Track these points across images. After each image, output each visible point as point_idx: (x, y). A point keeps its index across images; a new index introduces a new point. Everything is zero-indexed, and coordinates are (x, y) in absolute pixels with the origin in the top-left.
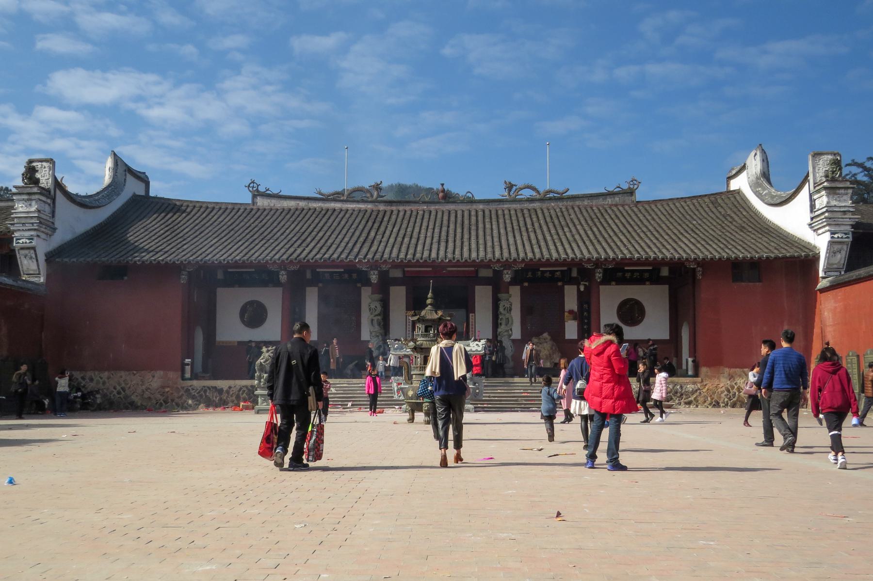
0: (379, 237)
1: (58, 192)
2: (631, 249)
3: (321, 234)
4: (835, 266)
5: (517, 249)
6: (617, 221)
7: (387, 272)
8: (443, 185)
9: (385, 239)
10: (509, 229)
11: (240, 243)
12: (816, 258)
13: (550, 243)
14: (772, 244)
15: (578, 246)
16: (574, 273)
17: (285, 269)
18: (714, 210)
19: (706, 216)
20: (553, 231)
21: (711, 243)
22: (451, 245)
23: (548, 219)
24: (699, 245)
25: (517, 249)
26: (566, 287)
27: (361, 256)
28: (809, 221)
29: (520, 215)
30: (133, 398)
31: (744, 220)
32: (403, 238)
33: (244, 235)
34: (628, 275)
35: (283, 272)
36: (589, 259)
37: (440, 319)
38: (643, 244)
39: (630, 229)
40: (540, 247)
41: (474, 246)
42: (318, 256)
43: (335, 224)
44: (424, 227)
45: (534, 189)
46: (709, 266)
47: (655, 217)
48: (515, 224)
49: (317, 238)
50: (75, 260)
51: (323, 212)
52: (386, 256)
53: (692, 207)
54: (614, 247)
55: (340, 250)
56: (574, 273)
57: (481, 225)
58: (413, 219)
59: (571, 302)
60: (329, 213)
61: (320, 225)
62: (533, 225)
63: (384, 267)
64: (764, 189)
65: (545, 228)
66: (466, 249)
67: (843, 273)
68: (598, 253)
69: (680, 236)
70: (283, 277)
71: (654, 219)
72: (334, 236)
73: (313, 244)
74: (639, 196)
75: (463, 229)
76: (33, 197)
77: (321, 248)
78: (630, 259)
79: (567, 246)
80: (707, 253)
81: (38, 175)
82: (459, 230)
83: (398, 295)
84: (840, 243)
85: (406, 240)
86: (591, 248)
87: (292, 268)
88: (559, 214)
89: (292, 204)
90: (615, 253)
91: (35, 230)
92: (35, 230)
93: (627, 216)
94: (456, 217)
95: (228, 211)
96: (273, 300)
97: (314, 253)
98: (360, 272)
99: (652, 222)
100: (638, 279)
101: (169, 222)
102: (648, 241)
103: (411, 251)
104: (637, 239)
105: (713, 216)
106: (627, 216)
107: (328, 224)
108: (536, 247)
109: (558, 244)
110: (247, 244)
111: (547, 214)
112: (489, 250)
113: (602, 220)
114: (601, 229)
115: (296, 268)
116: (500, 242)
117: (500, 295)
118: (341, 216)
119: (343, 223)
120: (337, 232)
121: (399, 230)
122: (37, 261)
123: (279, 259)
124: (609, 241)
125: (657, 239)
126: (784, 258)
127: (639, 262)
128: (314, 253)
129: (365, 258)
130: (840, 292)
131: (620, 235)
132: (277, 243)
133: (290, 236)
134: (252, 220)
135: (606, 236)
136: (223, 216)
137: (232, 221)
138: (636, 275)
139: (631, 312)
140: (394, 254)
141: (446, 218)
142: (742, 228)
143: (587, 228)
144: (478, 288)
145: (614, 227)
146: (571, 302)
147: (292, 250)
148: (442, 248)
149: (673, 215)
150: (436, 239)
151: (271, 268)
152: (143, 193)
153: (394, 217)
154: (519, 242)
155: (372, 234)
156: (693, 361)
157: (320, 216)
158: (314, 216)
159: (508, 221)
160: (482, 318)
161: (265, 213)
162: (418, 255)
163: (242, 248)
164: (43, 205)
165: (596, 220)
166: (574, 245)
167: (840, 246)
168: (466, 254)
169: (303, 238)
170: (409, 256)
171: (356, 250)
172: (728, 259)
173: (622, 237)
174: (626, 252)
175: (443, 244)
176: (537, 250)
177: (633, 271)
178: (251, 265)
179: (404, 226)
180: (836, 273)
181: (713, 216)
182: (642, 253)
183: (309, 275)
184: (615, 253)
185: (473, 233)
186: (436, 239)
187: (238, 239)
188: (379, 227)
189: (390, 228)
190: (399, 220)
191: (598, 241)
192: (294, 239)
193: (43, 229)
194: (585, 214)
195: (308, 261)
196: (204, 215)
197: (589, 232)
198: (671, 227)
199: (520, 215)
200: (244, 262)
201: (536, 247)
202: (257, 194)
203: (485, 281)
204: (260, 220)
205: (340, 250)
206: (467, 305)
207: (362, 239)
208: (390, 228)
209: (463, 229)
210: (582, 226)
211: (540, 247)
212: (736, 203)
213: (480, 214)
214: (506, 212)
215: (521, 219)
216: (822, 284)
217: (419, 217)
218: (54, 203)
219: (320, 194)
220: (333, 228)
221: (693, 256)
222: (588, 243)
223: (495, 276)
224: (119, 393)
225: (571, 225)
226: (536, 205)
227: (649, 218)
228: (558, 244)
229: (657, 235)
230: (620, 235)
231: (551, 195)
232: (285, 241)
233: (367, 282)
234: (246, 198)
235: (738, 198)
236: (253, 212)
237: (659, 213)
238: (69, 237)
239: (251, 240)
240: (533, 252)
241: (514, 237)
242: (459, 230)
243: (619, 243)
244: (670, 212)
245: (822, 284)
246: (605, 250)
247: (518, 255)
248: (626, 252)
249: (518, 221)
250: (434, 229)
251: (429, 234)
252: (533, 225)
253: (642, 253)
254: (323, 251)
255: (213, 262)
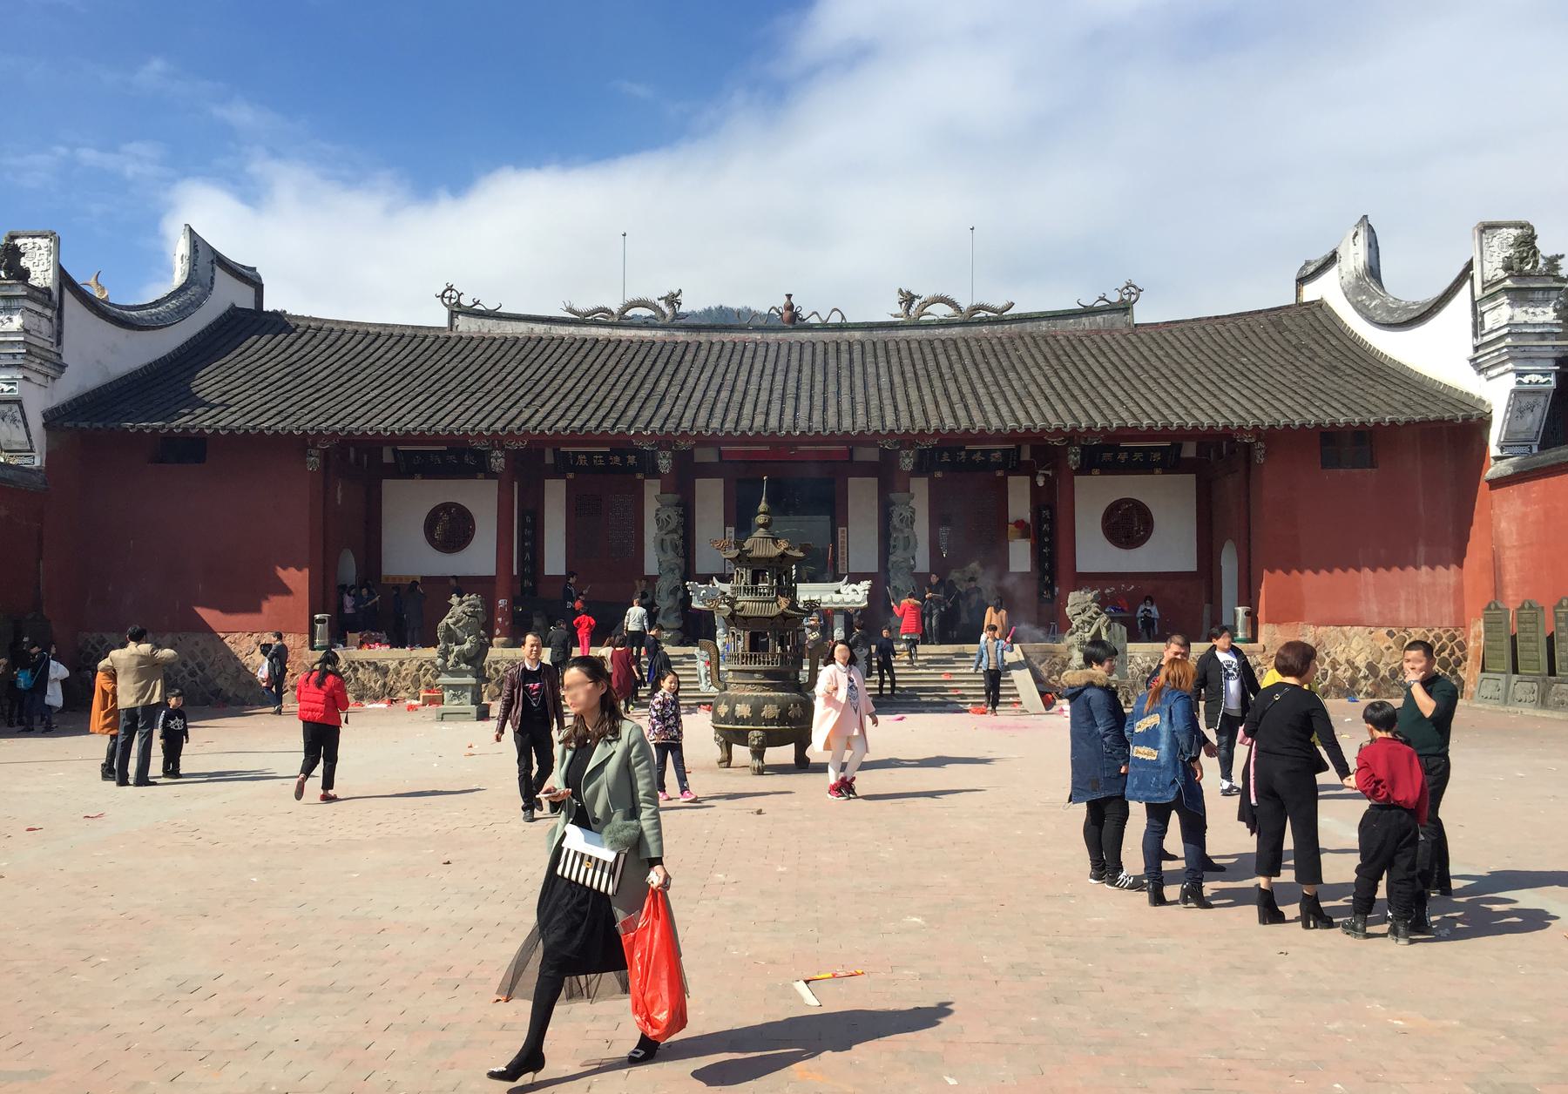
0: (674, 390)
1: (67, 295)
2: (1135, 410)
3: (569, 384)
4: (1522, 436)
5: (925, 412)
6: (1102, 359)
7: (690, 453)
8: (789, 296)
9: (684, 394)
10: (909, 375)
11: (420, 399)
12: (1485, 422)
13: (985, 400)
14: (1397, 397)
15: (1037, 405)
16: (1026, 455)
17: (502, 448)
18: (1277, 337)
19: (1262, 347)
20: (988, 379)
21: (1280, 396)
22: (804, 402)
23: (978, 357)
24: (1258, 401)
25: (925, 412)
26: (1011, 479)
27: (640, 425)
28: (1470, 353)
29: (927, 350)
30: (220, 682)
31: (1336, 354)
32: (718, 392)
33: (428, 383)
34: (1123, 457)
35: (497, 453)
36: (1058, 429)
37: (783, 555)
38: (1154, 400)
39: (1128, 374)
40: (966, 407)
41: (846, 405)
42: (561, 424)
43: (597, 366)
44: (756, 372)
45: (951, 303)
46: (1278, 438)
47: (1172, 352)
48: (919, 366)
49: (563, 391)
50: (100, 425)
51: (577, 345)
52: (686, 424)
53: (1236, 332)
54: (1102, 406)
55: (602, 412)
56: (1026, 455)
57: (858, 369)
58: (736, 358)
59: (1019, 506)
60: (588, 346)
61: (569, 368)
62: (951, 367)
63: (683, 445)
64: (1372, 298)
65: (974, 374)
66: (832, 411)
67: (1535, 450)
68: (1074, 417)
69: (1222, 385)
70: (498, 462)
71: (1167, 355)
72: (592, 388)
73: (553, 402)
74: (1144, 314)
75: (826, 374)
76: (15, 303)
77: (568, 409)
78: (1135, 428)
79: (1016, 405)
80: (1278, 416)
81: (24, 262)
82: (819, 377)
83: (710, 496)
84: (1533, 392)
85: (724, 394)
86: (1060, 408)
87: (514, 446)
88: (998, 348)
89: (521, 329)
90: (1104, 416)
91: (20, 366)
92: (20, 366)
93: (1119, 351)
94: (814, 354)
95: (406, 340)
96: (481, 501)
97: (553, 417)
98: (638, 452)
99: (1166, 360)
100: (1142, 463)
101: (295, 358)
102: (1163, 395)
103: (732, 415)
104: (1143, 390)
105: (1276, 348)
106: (1119, 351)
107: (585, 366)
108: (959, 408)
109: (1000, 402)
110: (433, 399)
111: (975, 349)
112: (874, 413)
113: (1075, 359)
114: (1075, 373)
115: (522, 445)
116: (894, 398)
117: (893, 496)
118: (608, 351)
119: (611, 363)
120: (598, 380)
121: (711, 378)
122: (26, 426)
123: (488, 429)
124: (1092, 395)
125: (1180, 391)
126: (1424, 423)
127: (1151, 434)
128: (553, 417)
129: (646, 429)
130: (1537, 487)
131: (1110, 383)
132: (487, 399)
133: (513, 387)
134: (448, 357)
135: (1085, 386)
136: (396, 349)
137: (411, 358)
138: (1138, 456)
139: (1127, 525)
140: (701, 422)
141: (795, 356)
142: (1333, 369)
143: (1049, 373)
144: (853, 482)
145: (1099, 370)
146: (1019, 506)
147: (514, 411)
148: (789, 411)
149: (1203, 347)
150: (776, 395)
151: (479, 445)
152: (250, 305)
153: (703, 354)
154: (928, 398)
155: (663, 383)
156: (1248, 614)
157: (572, 350)
158: (560, 350)
159: (906, 361)
160: (861, 539)
161: (472, 345)
162: (745, 423)
163: (422, 407)
164: (36, 319)
165: (1064, 358)
166: (1028, 403)
167: (1531, 399)
168: (832, 421)
169: (537, 390)
170: (729, 425)
171: (631, 413)
172: (1318, 426)
173: (1115, 389)
174: (1125, 415)
175: (790, 403)
176: (961, 413)
177: (1131, 451)
178: (436, 439)
179: (721, 370)
180: (1522, 450)
181: (1276, 348)
182: (1156, 417)
183: (549, 459)
184: (1104, 416)
185: (845, 384)
186: (776, 395)
187: (419, 390)
188: (676, 371)
189: (695, 373)
190: (712, 359)
191: (1073, 396)
192: (521, 392)
193: (34, 366)
194: (1046, 349)
195: (542, 432)
196: (360, 347)
197: (1054, 380)
198: (1203, 369)
199: (927, 350)
200: (422, 432)
201: (959, 408)
202: (456, 310)
203: (866, 470)
204: (462, 356)
205: (602, 412)
206: (834, 508)
207: (643, 394)
208: (695, 373)
209: (826, 374)
210: (1040, 368)
211: (966, 407)
212: (1316, 324)
213: (857, 348)
214: (903, 345)
215: (929, 357)
216: (1493, 470)
217: (748, 354)
218: (60, 317)
219: (570, 310)
220: (592, 372)
221: (1251, 422)
222: (1053, 399)
223: (883, 460)
224: (192, 674)
225: (1019, 367)
226: (955, 332)
227: (1160, 353)
228: (1000, 402)
229: (1179, 385)
230: (1110, 383)
231: (982, 314)
232: (504, 396)
233: (654, 472)
234: (438, 317)
235: (1320, 315)
236: (451, 343)
237: (1177, 345)
238: (93, 381)
239: (440, 393)
240: (955, 417)
241: (919, 388)
242: (819, 377)
243: (1110, 399)
244: (1197, 342)
245: (1493, 470)
246: (1085, 411)
247: (927, 422)
248: (1125, 415)
249: (925, 361)
250: (774, 375)
251: (766, 385)
252: (951, 367)
253: (1156, 417)
254: (570, 414)
255: (365, 433)
